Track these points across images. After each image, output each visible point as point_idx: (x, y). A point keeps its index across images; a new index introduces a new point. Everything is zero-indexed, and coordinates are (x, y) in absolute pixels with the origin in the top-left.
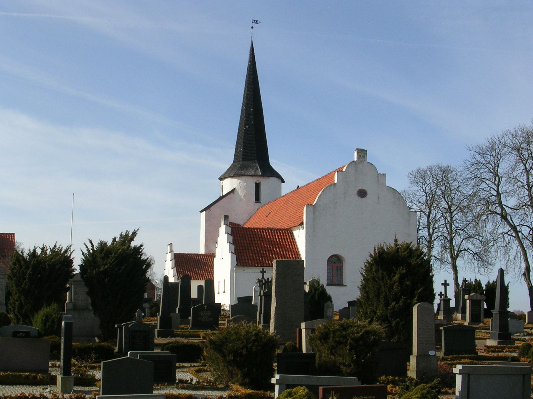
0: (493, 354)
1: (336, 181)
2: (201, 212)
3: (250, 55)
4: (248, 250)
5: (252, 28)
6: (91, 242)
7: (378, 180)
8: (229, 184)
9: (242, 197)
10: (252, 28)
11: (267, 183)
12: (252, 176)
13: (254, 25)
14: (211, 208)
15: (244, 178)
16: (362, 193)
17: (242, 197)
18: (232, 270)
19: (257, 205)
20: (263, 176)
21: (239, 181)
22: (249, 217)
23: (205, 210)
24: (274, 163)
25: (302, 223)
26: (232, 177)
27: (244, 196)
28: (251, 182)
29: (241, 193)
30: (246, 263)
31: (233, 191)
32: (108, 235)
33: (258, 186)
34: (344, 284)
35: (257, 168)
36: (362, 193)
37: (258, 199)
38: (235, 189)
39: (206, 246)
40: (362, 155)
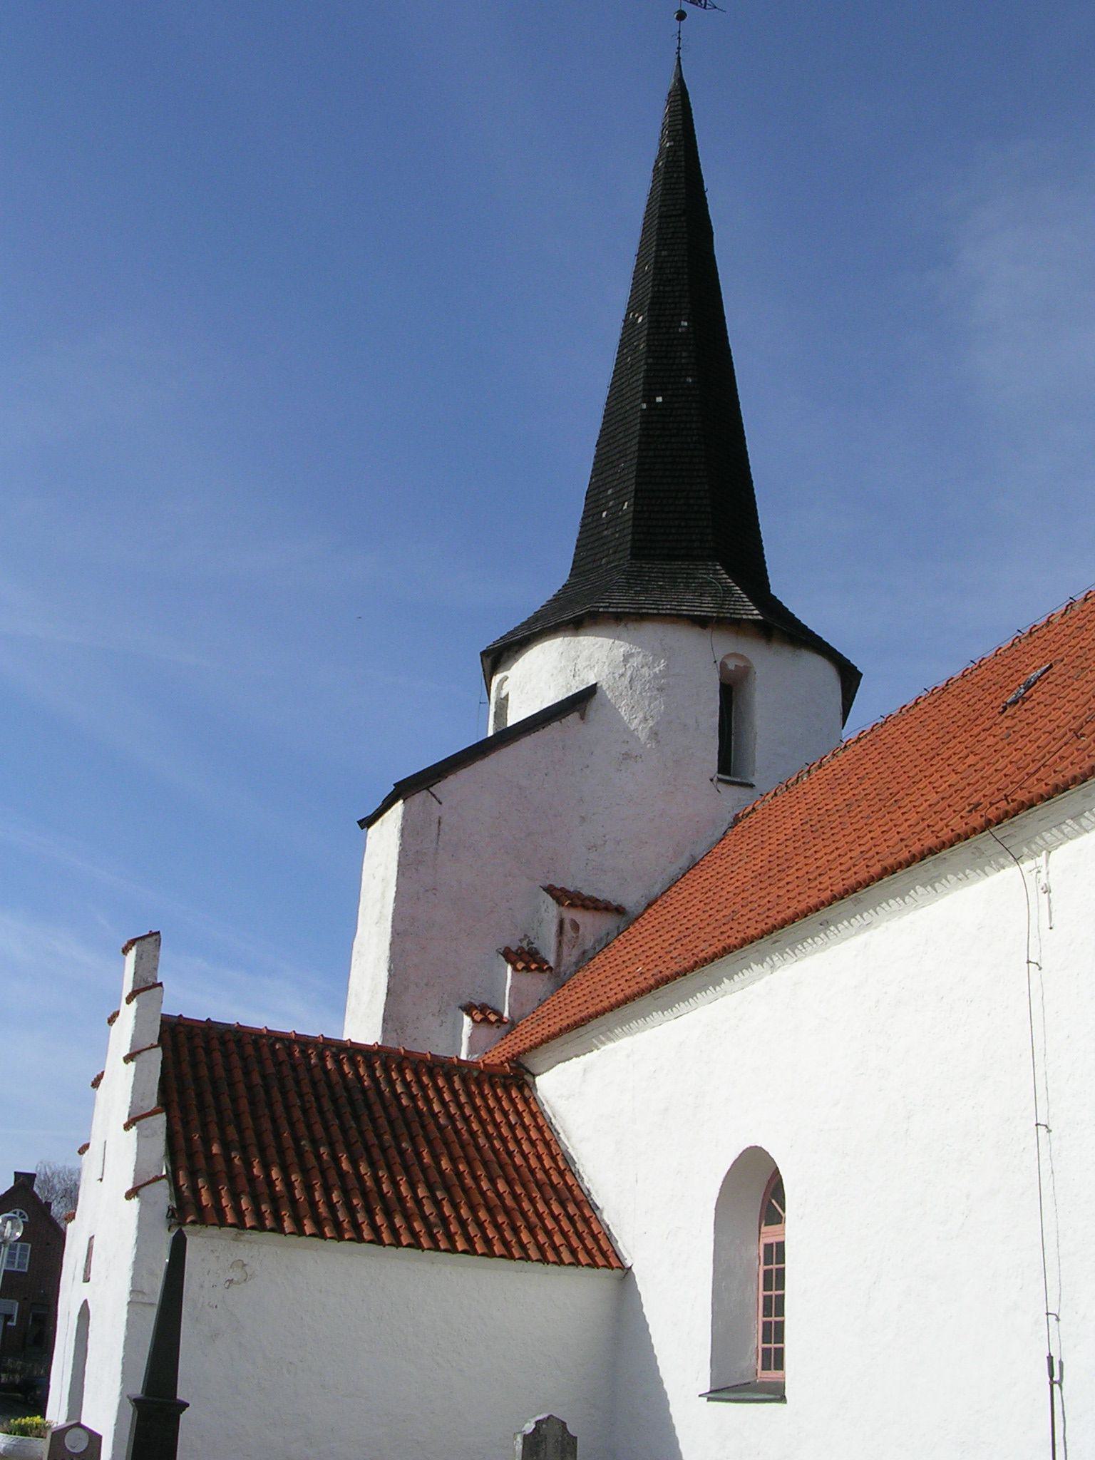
0: (262, 1092)
1: (384, 842)
3: (671, 114)
5: (681, 16)
6: (756, 1192)
9: (643, 736)
10: (681, 16)
11: (779, 679)
14: (442, 788)
15: (651, 631)
19: (731, 799)
22: (683, 862)
23: (403, 790)
24: (789, 584)
26: (576, 625)
27: (654, 734)
28: (699, 657)
29: (631, 713)
32: (100, 1432)
33: (731, 693)
35: (728, 591)
37: (729, 763)
38: (591, 691)
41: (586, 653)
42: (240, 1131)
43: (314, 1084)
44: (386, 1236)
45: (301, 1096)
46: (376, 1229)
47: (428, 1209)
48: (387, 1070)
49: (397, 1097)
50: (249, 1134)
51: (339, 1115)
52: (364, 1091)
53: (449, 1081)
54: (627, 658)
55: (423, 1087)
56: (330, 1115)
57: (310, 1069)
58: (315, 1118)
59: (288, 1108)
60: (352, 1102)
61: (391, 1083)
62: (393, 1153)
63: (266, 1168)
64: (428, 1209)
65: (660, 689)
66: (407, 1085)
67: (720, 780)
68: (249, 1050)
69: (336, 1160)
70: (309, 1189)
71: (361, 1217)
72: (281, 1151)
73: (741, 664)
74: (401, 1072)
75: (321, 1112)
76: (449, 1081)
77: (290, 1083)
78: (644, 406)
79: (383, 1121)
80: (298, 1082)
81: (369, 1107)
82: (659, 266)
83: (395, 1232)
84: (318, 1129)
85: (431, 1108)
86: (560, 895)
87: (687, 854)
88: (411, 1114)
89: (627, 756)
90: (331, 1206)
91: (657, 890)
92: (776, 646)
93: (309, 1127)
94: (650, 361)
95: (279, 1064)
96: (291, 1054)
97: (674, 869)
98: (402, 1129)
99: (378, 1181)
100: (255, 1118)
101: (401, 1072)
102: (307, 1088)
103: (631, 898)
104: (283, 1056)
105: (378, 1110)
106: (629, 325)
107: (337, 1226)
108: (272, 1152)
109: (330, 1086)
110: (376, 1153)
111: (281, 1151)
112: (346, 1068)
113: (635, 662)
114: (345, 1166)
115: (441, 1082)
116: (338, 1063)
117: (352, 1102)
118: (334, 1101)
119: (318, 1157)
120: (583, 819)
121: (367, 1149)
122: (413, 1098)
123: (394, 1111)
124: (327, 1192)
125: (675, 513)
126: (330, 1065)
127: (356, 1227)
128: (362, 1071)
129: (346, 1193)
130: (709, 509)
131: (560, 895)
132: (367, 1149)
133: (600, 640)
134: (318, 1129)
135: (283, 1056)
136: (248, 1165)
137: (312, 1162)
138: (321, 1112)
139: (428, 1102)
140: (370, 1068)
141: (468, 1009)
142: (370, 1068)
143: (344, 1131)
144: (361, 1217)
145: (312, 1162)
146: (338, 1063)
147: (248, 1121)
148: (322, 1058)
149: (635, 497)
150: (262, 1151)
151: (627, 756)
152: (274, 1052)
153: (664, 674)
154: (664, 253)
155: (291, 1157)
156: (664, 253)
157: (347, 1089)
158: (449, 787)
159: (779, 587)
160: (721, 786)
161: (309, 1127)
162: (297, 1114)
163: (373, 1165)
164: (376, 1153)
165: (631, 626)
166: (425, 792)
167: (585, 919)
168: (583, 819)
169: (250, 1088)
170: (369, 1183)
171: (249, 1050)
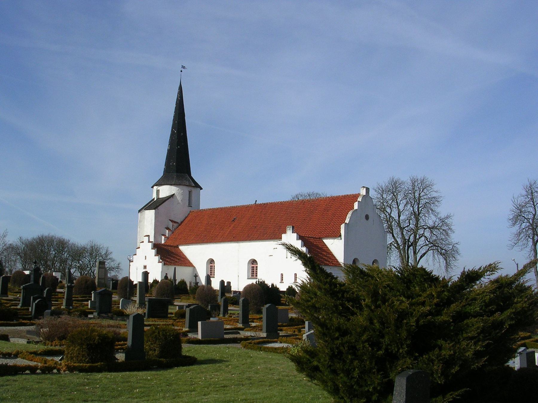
8: (165, 191)
13: (183, 70)
16: (367, 217)
17: (180, 201)
21: (178, 189)
25: (340, 236)
26: (171, 185)
28: (187, 189)
29: (179, 198)
31: (173, 196)
33: (190, 192)
86: (172, 221)
91: (182, 220)
103: (179, 221)
125: (178, 166)
131: (172, 221)
141: (163, 235)
159: (193, 175)
167: (175, 224)
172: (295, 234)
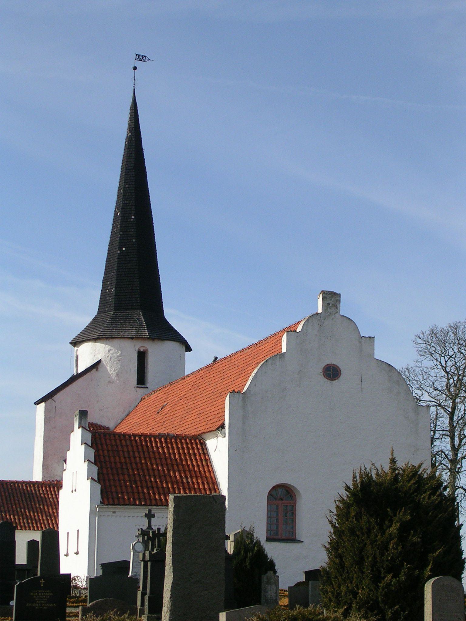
2: (37, 403)
3: (131, 119)
4: (123, 474)
7: (361, 348)
8: (89, 353)
9: (114, 376)
10: (135, 68)
11: (159, 353)
12: (132, 338)
13: (138, 64)
15: (116, 342)
16: (332, 372)
17: (114, 376)
18: (92, 513)
19: (141, 392)
20: (152, 338)
21: (108, 347)
22: (126, 413)
23: (44, 399)
25: (222, 426)
26: (96, 340)
27: (117, 375)
28: (131, 349)
30: (118, 498)
31: (96, 365)
33: (142, 356)
34: (298, 538)
35: (141, 325)
36: (332, 372)
37: (141, 380)
38: (100, 361)
39: (45, 466)
40: (332, 302)
41: (98, 349)
42: (4, 508)
43: (21, 494)
44: (36, 529)
45: (17, 497)
46: (33, 527)
47: (45, 521)
48: (38, 487)
49: (40, 494)
50: (6, 509)
51: (27, 501)
52: (33, 494)
53: (54, 488)
54: (109, 351)
55: (47, 491)
56: (24, 501)
57: (20, 489)
58: (21, 502)
59: (14, 500)
60: (30, 498)
61: (39, 491)
62: (39, 509)
63: (10, 516)
64: (45, 521)
65: (119, 361)
66: (43, 491)
67: (137, 387)
68: (5, 486)
69: (25, 512)
70: (19, 520)
71: (30, 525)
72: (13, 512)
73: (145, 349)
74: (42, 488)
75: (22, 501)
76: (54, 488)
77: (15, 495)
78: (119, 252)
79: (37, 502)
80: (17, 494)
81: (34, 498)
82: (125, 193)
83: (38, 528)
84: (22, 505)
85: (48, 496)
87: (127, 411)
88: (44, 499)
89: (109, 382)
90: (24, 523)
91: (119, 422)
92: (156, 341)
93: (20, 505)
94: (121, 233)
95: (12, 489)
96: (15, 486)
97: (123, 416)
98: (41, 503)
99: (35, 516)
100: (7, 504)
101: (42, 488)
102: (19, 495)
104: (13, 487)
105: (36, 498)
106: (116, 214)
107: (25, 527)
108: (11, 512)
109: (24, 494)
110: (35, 510)
111: (13, 512)
112: (28, 488)
113: (112, 352)
114: (27, 513)
115: (52, 489)
116: (27, 487)
117: (30, 498)
118: (25, 497)
119: (21, 512)
120: (98, 401)
121: (33, 509)
122: (44, 494)
123: (40, 499)
124: (23, 520)
125: (133, 295)
126: (24, 488)
127: (29, 527)
128: (32, 488)
129: (27, 520)
130: (139, 291)
132: (33, 509)
133: (102, 345)
134: (22, 505)
135: (13, 487)
136: (6, 516)
137: (20, 513)
138: (22, 501)
139: (48, 495)
140: (34, 487)
142: (34, 487)
143: (28, 505)
144: (30, 525)
145: (20, 513)
146: (27, 487)
147: (6, 505)
148: (22, 486)
149: (116, 287)
150: (9, 512)
151: (109, 382)
152: (11, 486)
153: (120, 356)
154: (127, 186)
155: (15, 512)
156: (127, 186)
157: (28, 494)
158: (57, 397)
160: (138, 388)
161: (20, 505)
162: (17, 502)
163: (34, 513)
164: (35, 510)
165: (110, 340)
166: (51, 399)
168: (98, 401)
169: (6, 497)
170: (32, 517)
171: (5, 486)
172: (81, 429)
